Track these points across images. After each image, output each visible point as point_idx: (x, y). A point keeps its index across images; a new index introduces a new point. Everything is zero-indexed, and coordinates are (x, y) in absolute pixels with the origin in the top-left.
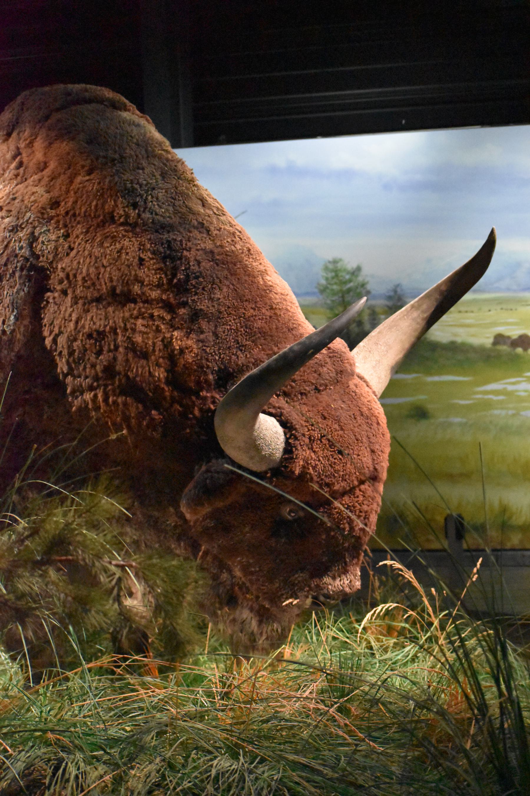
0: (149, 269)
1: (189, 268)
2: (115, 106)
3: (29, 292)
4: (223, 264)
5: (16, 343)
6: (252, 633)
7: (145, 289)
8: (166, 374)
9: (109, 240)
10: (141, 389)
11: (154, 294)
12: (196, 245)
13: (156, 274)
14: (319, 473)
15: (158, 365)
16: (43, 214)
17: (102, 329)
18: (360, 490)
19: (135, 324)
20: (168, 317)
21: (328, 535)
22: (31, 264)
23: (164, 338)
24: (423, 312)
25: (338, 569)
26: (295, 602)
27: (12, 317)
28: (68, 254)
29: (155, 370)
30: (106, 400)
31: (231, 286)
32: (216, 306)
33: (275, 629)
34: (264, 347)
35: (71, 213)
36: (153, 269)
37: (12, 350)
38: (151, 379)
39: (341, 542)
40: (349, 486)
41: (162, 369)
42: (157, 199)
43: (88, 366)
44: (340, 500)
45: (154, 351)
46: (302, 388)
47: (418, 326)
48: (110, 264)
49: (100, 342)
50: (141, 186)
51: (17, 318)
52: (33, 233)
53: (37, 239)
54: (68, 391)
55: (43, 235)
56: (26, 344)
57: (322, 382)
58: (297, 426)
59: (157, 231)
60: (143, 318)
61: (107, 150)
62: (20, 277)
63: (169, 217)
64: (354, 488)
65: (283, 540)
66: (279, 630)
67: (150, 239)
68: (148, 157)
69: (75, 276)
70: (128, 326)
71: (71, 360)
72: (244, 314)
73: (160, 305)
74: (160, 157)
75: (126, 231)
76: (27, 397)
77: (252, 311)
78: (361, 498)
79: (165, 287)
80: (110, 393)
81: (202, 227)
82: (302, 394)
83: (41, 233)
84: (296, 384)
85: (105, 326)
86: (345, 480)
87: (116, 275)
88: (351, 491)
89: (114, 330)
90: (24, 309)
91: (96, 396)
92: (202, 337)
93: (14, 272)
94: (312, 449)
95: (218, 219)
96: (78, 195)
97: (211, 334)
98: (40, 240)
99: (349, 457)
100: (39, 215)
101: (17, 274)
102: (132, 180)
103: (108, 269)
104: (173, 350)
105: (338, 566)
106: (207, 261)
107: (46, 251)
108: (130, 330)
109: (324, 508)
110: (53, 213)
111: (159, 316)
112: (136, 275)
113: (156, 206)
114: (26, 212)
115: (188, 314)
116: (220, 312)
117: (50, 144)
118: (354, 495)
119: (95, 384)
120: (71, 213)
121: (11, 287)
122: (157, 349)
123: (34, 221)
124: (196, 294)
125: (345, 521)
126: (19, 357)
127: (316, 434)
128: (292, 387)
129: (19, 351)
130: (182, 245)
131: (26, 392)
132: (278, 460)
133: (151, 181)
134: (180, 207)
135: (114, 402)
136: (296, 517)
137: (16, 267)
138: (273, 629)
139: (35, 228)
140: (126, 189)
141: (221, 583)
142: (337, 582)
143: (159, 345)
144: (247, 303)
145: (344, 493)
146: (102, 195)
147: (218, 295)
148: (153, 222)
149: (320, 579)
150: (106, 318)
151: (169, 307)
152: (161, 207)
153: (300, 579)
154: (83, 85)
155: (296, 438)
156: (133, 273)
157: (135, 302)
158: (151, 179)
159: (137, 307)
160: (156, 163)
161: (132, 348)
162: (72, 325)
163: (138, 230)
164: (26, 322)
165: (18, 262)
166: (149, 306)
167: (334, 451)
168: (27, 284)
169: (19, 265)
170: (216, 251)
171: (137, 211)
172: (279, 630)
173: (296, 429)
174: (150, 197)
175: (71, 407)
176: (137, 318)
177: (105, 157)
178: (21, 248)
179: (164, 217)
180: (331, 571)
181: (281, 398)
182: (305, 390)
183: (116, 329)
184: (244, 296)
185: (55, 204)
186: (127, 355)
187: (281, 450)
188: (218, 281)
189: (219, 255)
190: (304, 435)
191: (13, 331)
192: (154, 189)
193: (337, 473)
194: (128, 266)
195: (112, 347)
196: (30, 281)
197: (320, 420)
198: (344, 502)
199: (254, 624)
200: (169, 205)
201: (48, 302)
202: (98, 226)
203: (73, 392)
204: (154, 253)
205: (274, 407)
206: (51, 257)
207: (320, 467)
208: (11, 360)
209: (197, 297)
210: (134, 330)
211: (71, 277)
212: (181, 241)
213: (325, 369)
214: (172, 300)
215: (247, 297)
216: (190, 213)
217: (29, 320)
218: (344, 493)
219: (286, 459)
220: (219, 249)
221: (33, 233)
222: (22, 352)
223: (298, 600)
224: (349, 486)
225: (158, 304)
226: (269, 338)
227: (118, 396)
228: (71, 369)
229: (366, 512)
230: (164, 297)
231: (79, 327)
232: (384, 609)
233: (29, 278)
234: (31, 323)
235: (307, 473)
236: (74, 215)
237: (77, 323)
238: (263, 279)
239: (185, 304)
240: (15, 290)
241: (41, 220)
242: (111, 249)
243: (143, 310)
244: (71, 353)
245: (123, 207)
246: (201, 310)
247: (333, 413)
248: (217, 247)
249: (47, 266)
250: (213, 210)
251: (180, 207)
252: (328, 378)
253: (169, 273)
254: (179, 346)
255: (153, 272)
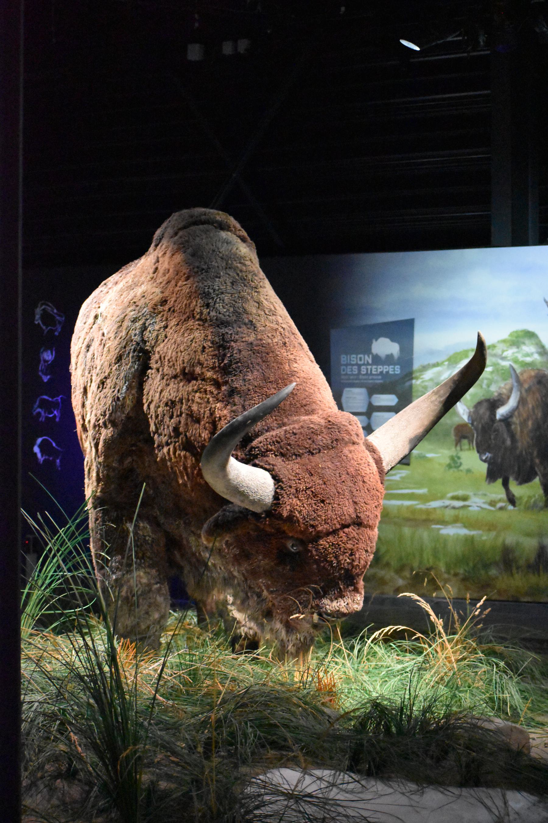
0: (208, 356)
1: (232, 356)
2: (223, 227)
3: (138, 369)
4: (258, 353)
5: (126, 407)
6: (282, 640)
7: (204, 370)
8: (209, 435)
9: (188, 331)
10: (194, 447)
11: (209, 374)
12: (242, 338)
13: (212, 359)
14: (304, 516)
15: (205, 428)
16: (154, 309)
17: (174, 399)
18: (344, 532)
19: (194, 396)
20: (215, 392)
21: (318, 565)
22: (141, 348)
23: (211, 408)
24: (440, 397)
25: (334, 593)
26: (302, 616)
27: (125, 387)
28: (164, 341)
29: (202, 432)
30: (174, 453)
31: (261, 370)
32: (247, 385)
33: (299, 638)
34: (277, 418)
35: (172, 309)
36: (210, 355)
37: (123, 413)
38: (200, 438)
39: (332, 571)
40: (332, 528)
41: (207, 432)
42: (223, 301)
43: (166, 427)
44: (325, 538)
45: (204, 417)
46: (296, 451)
47: (436, 408)
48: (185, 350)
49: (172, 409)
50: (214, 290)
51: (128, 389)
52: (145, 324)
53: (147, 329)
54: (155, 446)
55: (151, 325)
56: (132, 409)
57: (315, 447)
58: (284, 480)
59: (218, 326)
60: (200, 392)
61: (200, 262)
62: (133, 357)
63: (228, 316)
64: (338, 530)
65: (288, 568)
66: (302, 639)
67: (212, 332)
68: (226, 268)
69: (164, 359)
70: (190, 398)
71: (157, 421)
72: (266, 392)
73: (212, 383)
74: (235, 269)
75: (199, 325)
76: (134, 448)
77: (273, 390)
78: (345, 539)
79: (217, 369)
80: (178, 448)
81: (251, 325)
82: (296, 455)
83: (150, 324)
84: (291, 448)
85: (176, 397)
86: (328, 524)
87: (187, 358)
88: (335, 532)
89: (181, 401)
90: (133, 382)
91: (169, 449)
92: (234, 408)
93: (129, 353)
94: (298, 497)
95: (267, 318)
96: (178, 295)
97: (241, 406)
98: (149, 329)
99: (330, 506)
100: (152, 310)
101: (131, 355)
102: (209, 286)
103: (183, 354)
104: (215, 418)
105: (334, 590)
106: (246, 351)
107: (151, 338)
108: (191, 401)
109: (313, 544)
110: (160, 308)
111: (210, 391)
112: (199, 359)
113: (221, 307)
114: (144, 307)
115: (228, 391)
116: (249, 390)
117: (173, 255)
118: (338, 535)
119: (169, 441)
120: (172, 309)
121: (126, 364)
122: (206, 416)
123: (147, 314)
124: (235, 375)
125: (331, 556)
126: (128, 418)
127: (302, 487)
128: (287, 449)
129: (128, 414)
130: (231, 337)
131: (133, 445)
132: (270, 505)
133: (222, 287)
134: (238, 308)
135: (179, 455)
136: (297, 551)
137: (131, 350)
138: (297, 638)
139: (147, 319)
140: (204, 293)
141: (263, 600)
142: (335, 604)
143: (207, 413)
144: (270, 384)
145: (328, 534)
146: (190, 297)
147: (250, 376)
148: (216, 319)
149: (319, 600)
150: (178, 391)
151: (217, 385)
152: (224, 307)
153: (305, 599)
154: (203, 210)
155: (282, 488)
156: (197, 357)
157: (196, 379)
158: (223, 286)
159: (198, 384)
160: (231, 274)
161: (191, 415)
162: (158, 395)
163: (206, 325)
164: (134, 392)
165: (132, 345)
166: (205, 383)
167: (317, 500)
168: (137, 363)
169: (133, 347)
170: (255, 343)
171: (208, 310)
172: (302, 639)
173: (282, 482)
174: (218, 300)
175: (157, 458)
176: (196, 392)
177: (198, 267)
178: (135, 335)
179: (224, 316)
180: (329, 595)
181: (278, 457)
182: (299, 452)
183: (182, 400)
184: (269, 378)
185: (164, 302)
186: (187, 420)
187: (271, 497)
188: (251, 366)
189: (256, 346)
190: (291, 487)
191: (124, 398)
192: (222, 293)
193: (320, 518)
194: (195, 352)
195: (179, 413)
196: (139, 360)
197: (308, 476)
198: (329, 541)
199: (283, 633)
200: (230, 306)
201: (148, 377)
202: (185, 320)
203: (159, 446)
204: (212, 343)
205: (269, 464)
206: (153, 342)
207: (304, 512)
208: (122, 420)
209: (235, 377)
210: (193, 401)
211: (162, 359)
212: (231, 334)
213: (320, 437)
214: (220, 379)
215: (271, 380)
216: (244, 312)
217: (136, 390)
218: (328, 534)
219: (275, 504)
220: (259, 342)
221: (145, 324)
222: (131, 414)
223: (304, 615)
224: (332, 528)
225: (210, 382)
226: (282, 412)
227: (181, 451)
228: (157, 429)
229: (352, 550)
230: (215, 377)
231: (161, 397)
232: (392, 630)
233: (139, 357)
234: (137, 392)
235: (294, 516)
236: (174, 311)
237: (161, 393)
238: (289, 366)
239: (226, 383)
240: (128, 367)
241: (152, 314)
242: (188, 338)
243: (201, 386)
244: (157, 417)
245: (200, 307)
246: (236, 388)
247: (319, 471)
248: (257, 340)
249: (150, 349)
250: (264, 311)
251: (238, 308)
252: (321, 444)
253: (220, 358)
254: (219, 414)
255: (211, 357)
